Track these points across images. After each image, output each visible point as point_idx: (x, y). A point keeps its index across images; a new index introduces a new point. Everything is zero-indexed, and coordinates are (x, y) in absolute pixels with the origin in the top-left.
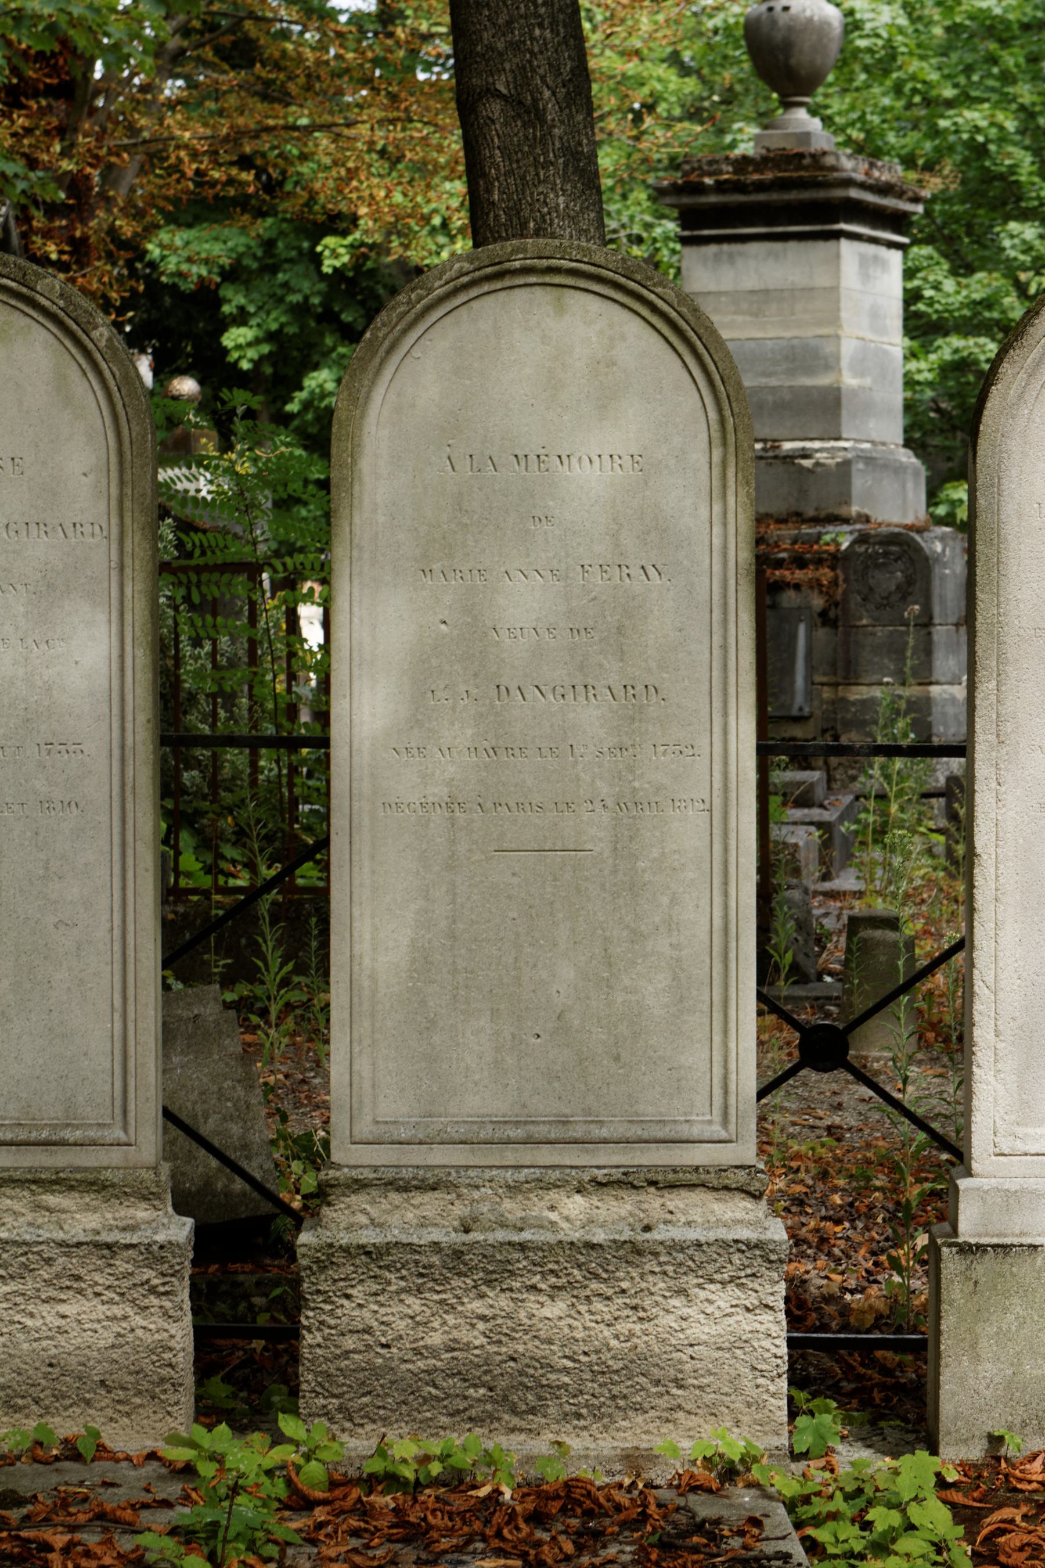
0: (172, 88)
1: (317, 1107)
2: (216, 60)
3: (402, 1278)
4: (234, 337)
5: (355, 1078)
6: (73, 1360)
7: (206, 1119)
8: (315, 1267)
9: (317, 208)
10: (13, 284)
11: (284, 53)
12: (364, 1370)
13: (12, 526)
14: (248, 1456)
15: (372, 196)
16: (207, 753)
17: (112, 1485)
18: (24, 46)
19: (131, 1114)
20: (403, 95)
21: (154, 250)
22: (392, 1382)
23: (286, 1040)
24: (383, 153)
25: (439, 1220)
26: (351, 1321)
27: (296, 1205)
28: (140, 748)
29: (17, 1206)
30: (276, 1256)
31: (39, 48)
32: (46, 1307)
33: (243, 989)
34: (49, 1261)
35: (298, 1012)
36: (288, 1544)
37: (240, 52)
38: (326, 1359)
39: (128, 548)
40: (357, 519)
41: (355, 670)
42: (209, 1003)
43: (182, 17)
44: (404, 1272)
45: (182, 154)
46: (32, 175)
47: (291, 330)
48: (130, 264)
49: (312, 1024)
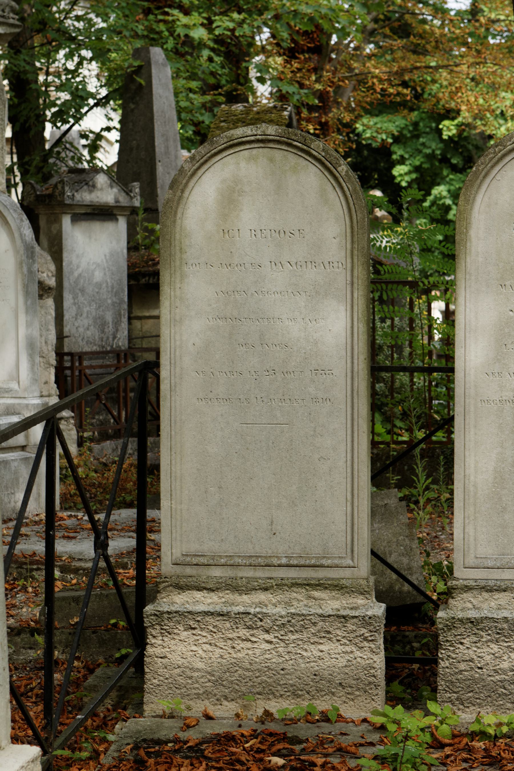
0: (370, 48)
1: (443, 550)
2: (391, 34)
3: (489, 635)
4: (398, 170)
5: (466, 536)
6: (326, 673)
7: (391, 555)
8: (445, 629)
9: (440, 106)
10: (300, 145)
11: (425, 31)
12: (469, 680)
13: (299, 263)
14: (413, 721)
15: (468, 101)
16: (388, 375)
17: (345, 734)
18: (297, 28)
19: (356, 552)
20: (483, 50)
21: (359, 127)
22: (483, 686)
23: (428, 517)
24: (473, 79)
25: (507, 606)
26: (463, 656)
27: (435, 597)
28: (361, 372)
29: (299, 597)
30: (425, 623)
31: (305, 29)
32: (312, 647)
33: (406, 491)
34: (315, 624)
35: (433, 503)
36: (432, 765)
37: (403, 30)
38: (451, 674)
39: (356, 274)
40: (468, 260)
41: (467, 334)
42: (392, 497)
43: (374, 14)
44: (490, 632)
45: (375, 80)
46: (302, 91)
47: (426, 166)
48: (348, 135)
49: (445, 508)
